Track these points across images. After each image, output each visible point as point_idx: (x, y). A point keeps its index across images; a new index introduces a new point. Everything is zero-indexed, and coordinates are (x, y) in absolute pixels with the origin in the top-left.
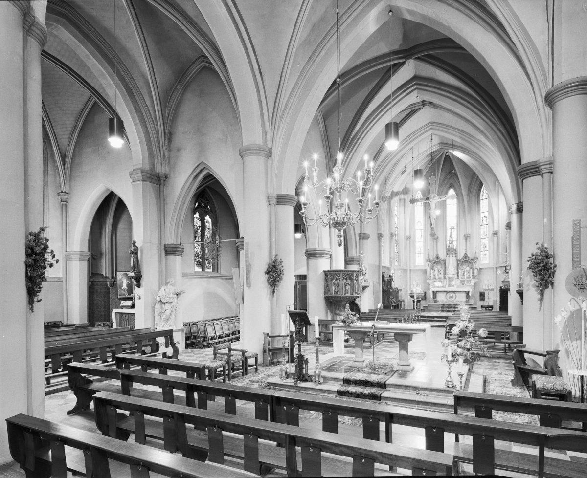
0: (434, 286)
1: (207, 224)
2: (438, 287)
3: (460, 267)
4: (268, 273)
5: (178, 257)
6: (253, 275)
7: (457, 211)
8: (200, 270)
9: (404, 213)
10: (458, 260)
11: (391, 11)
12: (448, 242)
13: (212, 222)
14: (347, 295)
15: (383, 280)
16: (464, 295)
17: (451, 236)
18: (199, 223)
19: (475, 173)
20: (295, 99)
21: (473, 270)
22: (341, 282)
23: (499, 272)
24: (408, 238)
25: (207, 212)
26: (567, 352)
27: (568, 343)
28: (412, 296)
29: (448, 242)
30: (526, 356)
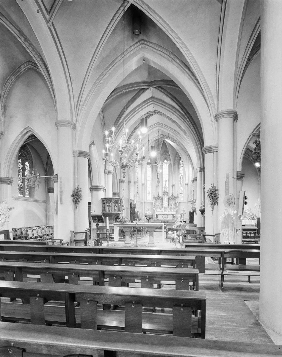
0: (157, 211)
1: (26, 167)
2: (159, 212)
3: (170, 201)
4: (73, 196)
5: (9, 186)
6: (64, 197)
7: (168, 172)
8: (22, 196)
9: (142, 171)
10: (169, 198)
11: (144, 60)
12: (164, 188)
13: (29, 166)
14: (115, 212)
15: (131, 207)
16: (172, 216)
17: (165, 184)
18: (21, 166)
19: (177, 153)
20: (91, 98)
21: (176, 203)
22: (112, 205)
23: (189, 204)
24: (143, 185)
25: (27, 159)
26: (223, 234)
27: (223, 230)
28: (146, 216)
29: (164, 188)
30: (206, 237)
